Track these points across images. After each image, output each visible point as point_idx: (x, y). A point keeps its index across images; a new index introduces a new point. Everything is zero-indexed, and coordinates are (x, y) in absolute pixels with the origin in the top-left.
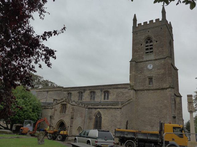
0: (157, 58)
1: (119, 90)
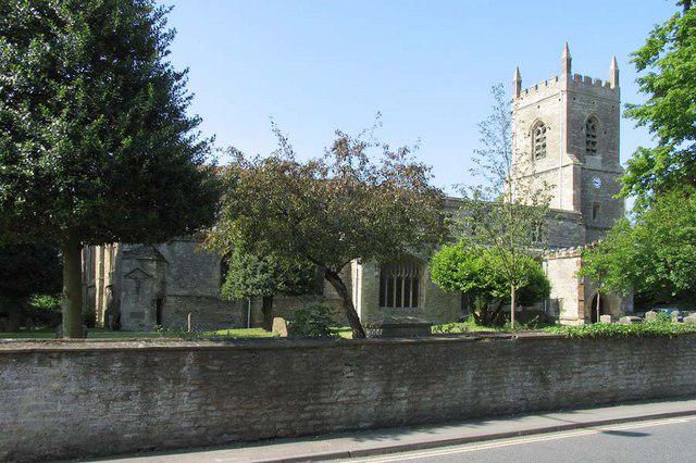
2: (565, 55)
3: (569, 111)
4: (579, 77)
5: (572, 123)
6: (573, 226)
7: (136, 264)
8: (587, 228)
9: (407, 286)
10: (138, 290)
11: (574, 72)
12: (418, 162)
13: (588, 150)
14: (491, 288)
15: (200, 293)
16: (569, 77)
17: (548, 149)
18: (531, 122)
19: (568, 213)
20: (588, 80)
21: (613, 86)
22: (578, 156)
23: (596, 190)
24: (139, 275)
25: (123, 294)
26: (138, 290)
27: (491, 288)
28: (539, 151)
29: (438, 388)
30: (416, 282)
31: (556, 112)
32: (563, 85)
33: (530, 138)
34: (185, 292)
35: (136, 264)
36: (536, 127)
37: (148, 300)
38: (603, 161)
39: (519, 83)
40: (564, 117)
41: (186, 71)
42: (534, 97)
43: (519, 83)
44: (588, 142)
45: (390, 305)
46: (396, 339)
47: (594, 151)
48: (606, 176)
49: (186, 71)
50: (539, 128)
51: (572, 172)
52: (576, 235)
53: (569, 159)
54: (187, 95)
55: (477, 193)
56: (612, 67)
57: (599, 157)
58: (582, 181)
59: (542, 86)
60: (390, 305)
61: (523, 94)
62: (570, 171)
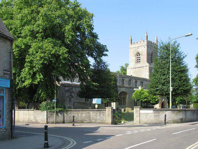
2: (146, 35)
3: (147, 51)
5: (148, 54)
7: (69, 94)
9: (123, 99)
10: (70, 101)
11: (148, 40)
14: (150, 101)
15: (81, 101)
16: (147, 41)
17: (141, 60)
18: (136, 52)
19: (148, 79)
20: (151, 42)
22: (149, 63)
24: (70, 97)
25: (66, 102)
26: (70, 101)
27: (150, 101)
28: (138, 61)
30: (125, 98)
31: (144, 50)
32: (146, 43)
33: (135, 57)
34: (78, 101)
35: (69, 94)
36: (137, 54)
37: (72, 103)
39: (131, 40)
40: (146, 52)
41: (99, 39)
42: (137, 45)
43: (131, 40)
45: (120, 105)
49: (99, 39)
50: (138, 54)
51: (148, 68)
53: (148, 64)
54: (185, 55)
56: (156, 39)
59: (139, 43)
60: (120, 105)
61: (133, 44)
62: (148, 68)
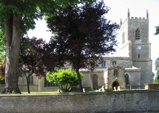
0: (143, 43)
1: (124, 61)
3: (129, 28)
4: (132, 18)
6: (127, 61)
8: (133, 61)
11: (131, 16)
12: (105, 18)
13: (136, 39)
20: (136, 18)
21: (146, 19)
23: (139, 50)
29: (72, 75)
38: (142, 41)
44: (136, 36)
46: (154, 78)
47: (139, 39)
48: (143, 45)
52: (129, 64)
55: (103, 54)
57: (141, 40)
58: (133, 48)
